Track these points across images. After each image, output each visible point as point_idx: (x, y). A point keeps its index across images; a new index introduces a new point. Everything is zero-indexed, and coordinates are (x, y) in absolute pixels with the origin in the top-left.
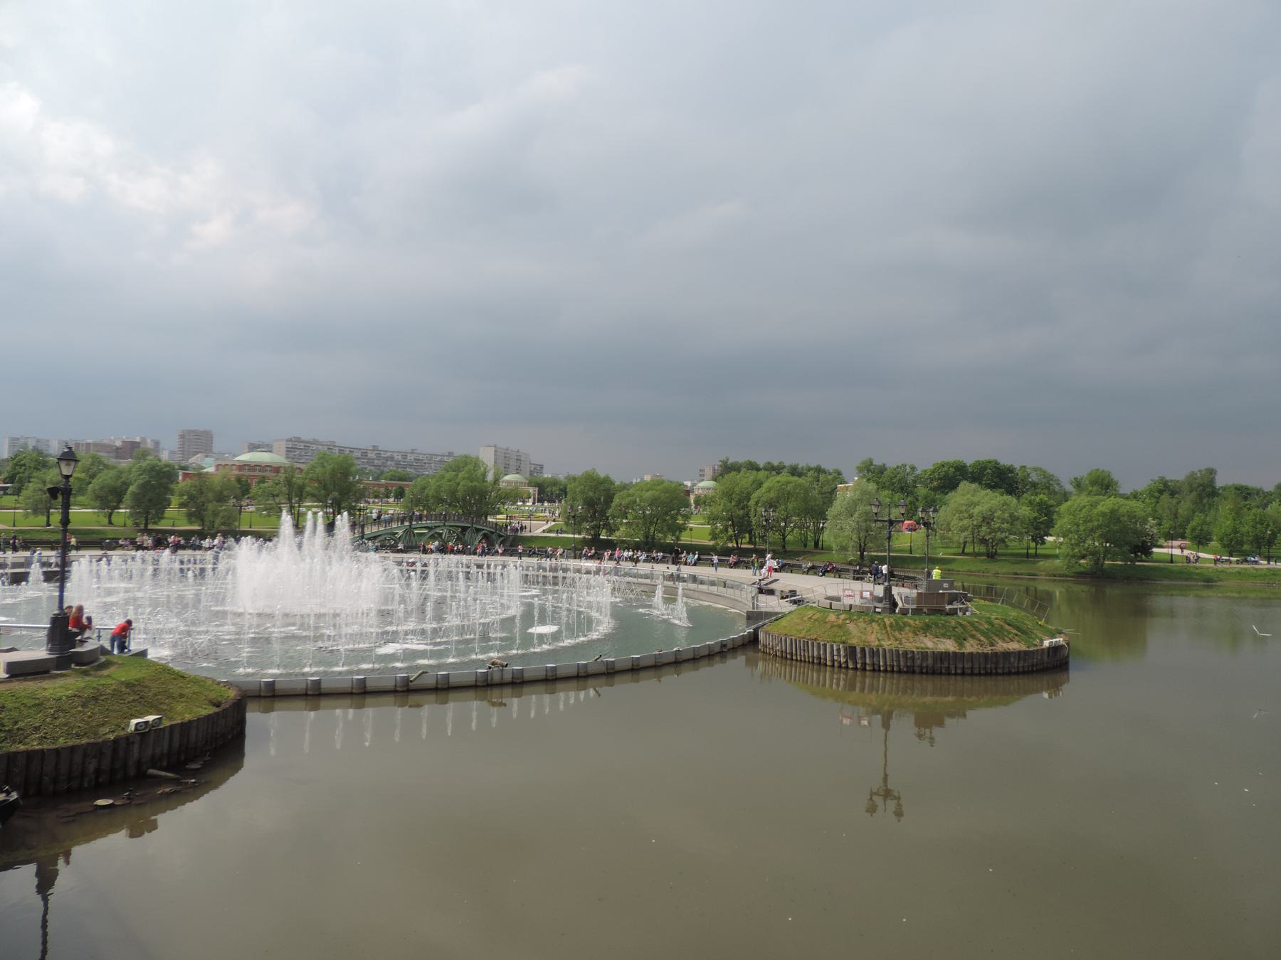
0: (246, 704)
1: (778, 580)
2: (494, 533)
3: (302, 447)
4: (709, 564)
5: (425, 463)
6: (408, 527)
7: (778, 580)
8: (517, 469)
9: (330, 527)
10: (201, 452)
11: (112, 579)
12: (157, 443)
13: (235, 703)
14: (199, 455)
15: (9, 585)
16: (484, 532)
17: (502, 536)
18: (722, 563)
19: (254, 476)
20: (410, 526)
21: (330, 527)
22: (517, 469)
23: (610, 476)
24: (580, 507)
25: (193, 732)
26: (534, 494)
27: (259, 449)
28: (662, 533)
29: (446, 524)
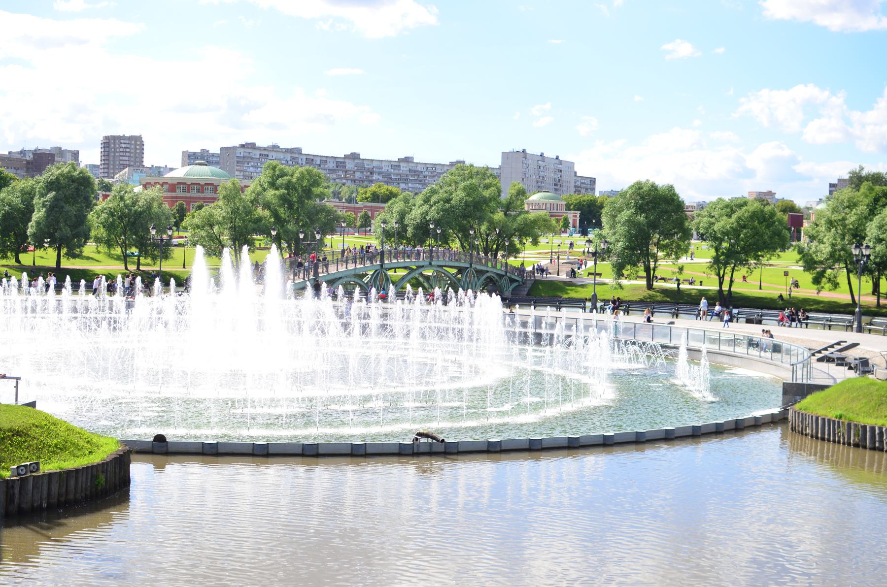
0: (129, 457)
1: (857, 344)
2: (503, 276)
3: (258, 156)
4: (824, 325)
5: (425, 177)
6: (379, 267)
7: (857, 344)
8: (556, 185)
9: (258, 268)
10: (129, 166)
11: (477, 372)
12: (75, 154)
13: (115, 458)
14: (126, 170)
15: (434, 391)
16: (488, 274)
17: (516, 281)
18: (710, 313)
19: (190, 198)
20: (382, 266)
21: (258, 268)
22: (556, 185)
23: (678, 190)
24: (301, 236)
25: (72, 482)
26: (574, 221)
27: (197, 162)
28: (155, 254)
29: (674, 286)
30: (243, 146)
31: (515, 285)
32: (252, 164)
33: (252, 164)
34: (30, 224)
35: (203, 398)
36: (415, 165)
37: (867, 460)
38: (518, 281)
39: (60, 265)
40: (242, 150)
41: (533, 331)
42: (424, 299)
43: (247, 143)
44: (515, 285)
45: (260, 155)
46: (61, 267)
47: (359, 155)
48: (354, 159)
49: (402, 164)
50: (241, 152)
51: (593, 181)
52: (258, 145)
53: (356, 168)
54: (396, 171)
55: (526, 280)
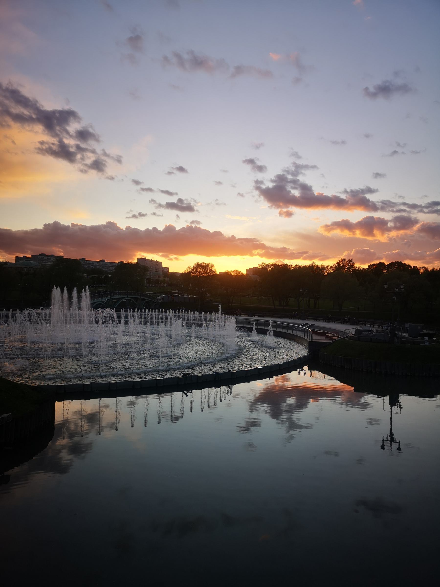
2: (151, 301)
20: (111, 298)
29: (128, 296)
30: (40, 255)
31: (155, 304)
32: (44, 261)
33: (44, 261)
34: (219, 312)
35: (376, 189)
36: (105, 263)
37: (437, 250)
38: (156, 302)
39: (61, 399)
40: (40, 256)
41: (46, 353)
42: (143, 326)
43: (42, 254)
44: (155, 304)
45: (47, 258)
46: (56, 402)
47: (85, 259)
48: (83, 260)
49: (101, 262)
50: (40, 257)
51: (168, 268)
52: (46, 254)
53: (84, 263)
54: (99, 265)
55: (159, 302)
